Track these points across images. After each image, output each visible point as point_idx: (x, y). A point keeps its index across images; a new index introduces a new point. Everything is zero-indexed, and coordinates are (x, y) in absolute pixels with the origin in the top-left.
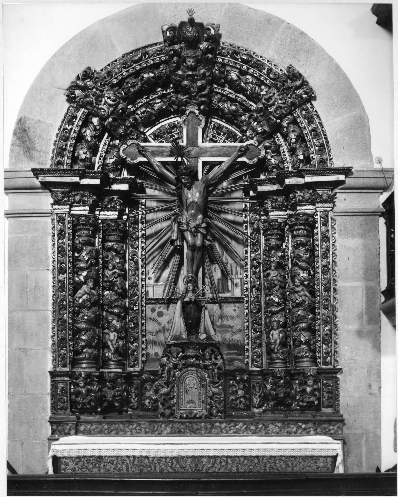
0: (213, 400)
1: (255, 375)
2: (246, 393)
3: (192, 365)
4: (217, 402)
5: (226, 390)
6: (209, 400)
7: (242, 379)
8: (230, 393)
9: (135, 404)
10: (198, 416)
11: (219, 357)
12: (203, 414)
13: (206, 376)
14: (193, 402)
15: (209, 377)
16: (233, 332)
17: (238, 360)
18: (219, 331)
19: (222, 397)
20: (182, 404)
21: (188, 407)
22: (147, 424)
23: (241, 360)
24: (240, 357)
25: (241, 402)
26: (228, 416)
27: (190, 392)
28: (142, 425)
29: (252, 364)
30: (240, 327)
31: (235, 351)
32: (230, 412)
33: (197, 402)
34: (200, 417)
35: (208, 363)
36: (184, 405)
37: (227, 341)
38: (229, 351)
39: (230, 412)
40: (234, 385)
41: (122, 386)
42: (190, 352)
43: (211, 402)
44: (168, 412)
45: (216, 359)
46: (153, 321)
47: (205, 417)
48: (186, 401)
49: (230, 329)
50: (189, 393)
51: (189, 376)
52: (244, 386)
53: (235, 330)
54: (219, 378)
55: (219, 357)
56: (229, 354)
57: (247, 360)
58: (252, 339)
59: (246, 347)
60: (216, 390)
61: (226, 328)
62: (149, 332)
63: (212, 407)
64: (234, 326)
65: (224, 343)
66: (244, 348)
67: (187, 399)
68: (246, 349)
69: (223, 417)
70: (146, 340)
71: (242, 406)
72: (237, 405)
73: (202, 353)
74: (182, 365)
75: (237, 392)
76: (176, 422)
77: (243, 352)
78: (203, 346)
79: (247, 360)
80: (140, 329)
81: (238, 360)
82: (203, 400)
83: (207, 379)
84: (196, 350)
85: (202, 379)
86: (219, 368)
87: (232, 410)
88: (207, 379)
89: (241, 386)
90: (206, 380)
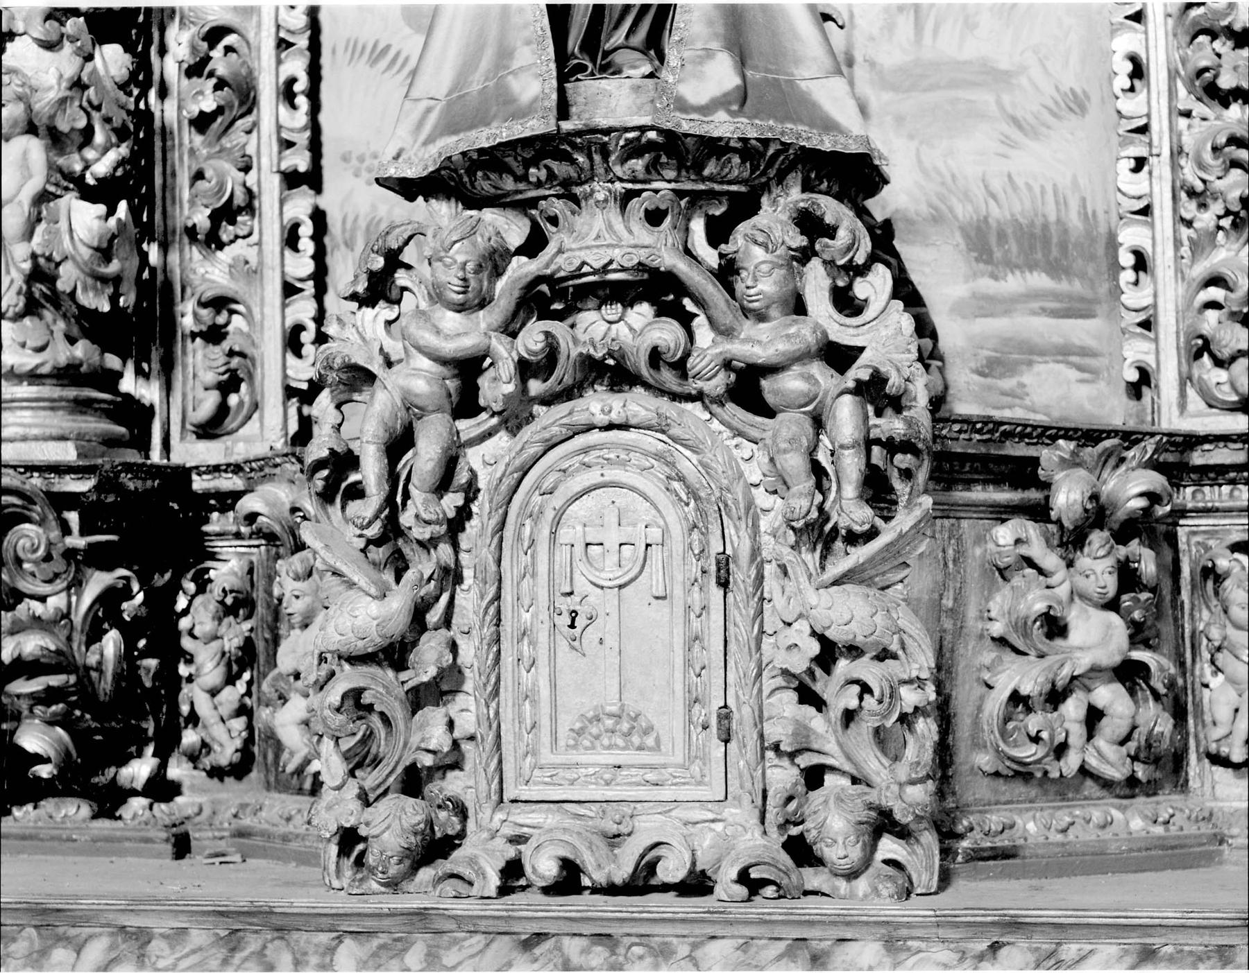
0: (819, 704)
1: (1216, 474)
2: (1139, 635)
3: (614, 372)
4: (866, 725)
5: (955, 613)
6: (786, 704)
7: (1098, 513)
8: (1002, 641)
9: (218, 731)
10: (672, 869)
11: (875, 286)
12: (725, 847)
13: (754, 474)
14: (630, 726)
15: (781, 485)
16: (1016, 122)
17: (1064, 353)
18: (900, 120)
19: (918, 682)
20: (532, 751)
21: (589, 771)
22: (198, 937)
23: (1085, 352)
24: (1079, 331)
25: (1094, 716)
26: (977, 856)
27: (606, 626)
28: (157, 946)
29: (1185, 380)
30: (1070, 81)
31: (1040, 280)
32: (995, 820)
33: (668, 718)
34: (697, 884)
35: (759, 343)
36: (546, 756)
37: (966, 197)
38: (986, 285)
39: (995, 820)
40: (1030, 562)
41: (77, 584)
42: (600, 236)
43: (802, 730)
44: (393, 824)
45: (846, 302)
46: (374, 61)
47: (743, 877)
48: (567, 722)
49: (985, 98)
50: (592, 635)
51: (592, 477)
52: (1128, 577)
53: (1027, 105)
54: (877, 490)
55: (875, 286)
56: (986, 306)
57: (1137, 350)
58: (1175, 167)
59: (1132, 236)
60: (849, 612)
61: (953, 84)
62: (345, 158)
63: (814, 777)
64: (1023, 69)
65: (937, 219)
66: (1113, 244)
67: (575, 705)
68: (1127, 259)
69: (925, 878)
70: (319, 217)
71: (1109, 758)
72: (1060, 750)
73: (711, 257)
74: (525, 369)
75: (1055, 627)
76: (470, 925)
77: (1104, 288)
78: (715, 176)
79: (1137, 350)
80: (267, 125)
81: (1064, 353)
82: (725, 715)
83: (762, 499)
84: (654, 218)
85: (706, 505)
86: (876, 393)
87: (1019, 788)
88: (762, 499)
89: (1097, 566)
90: (752, 513)
